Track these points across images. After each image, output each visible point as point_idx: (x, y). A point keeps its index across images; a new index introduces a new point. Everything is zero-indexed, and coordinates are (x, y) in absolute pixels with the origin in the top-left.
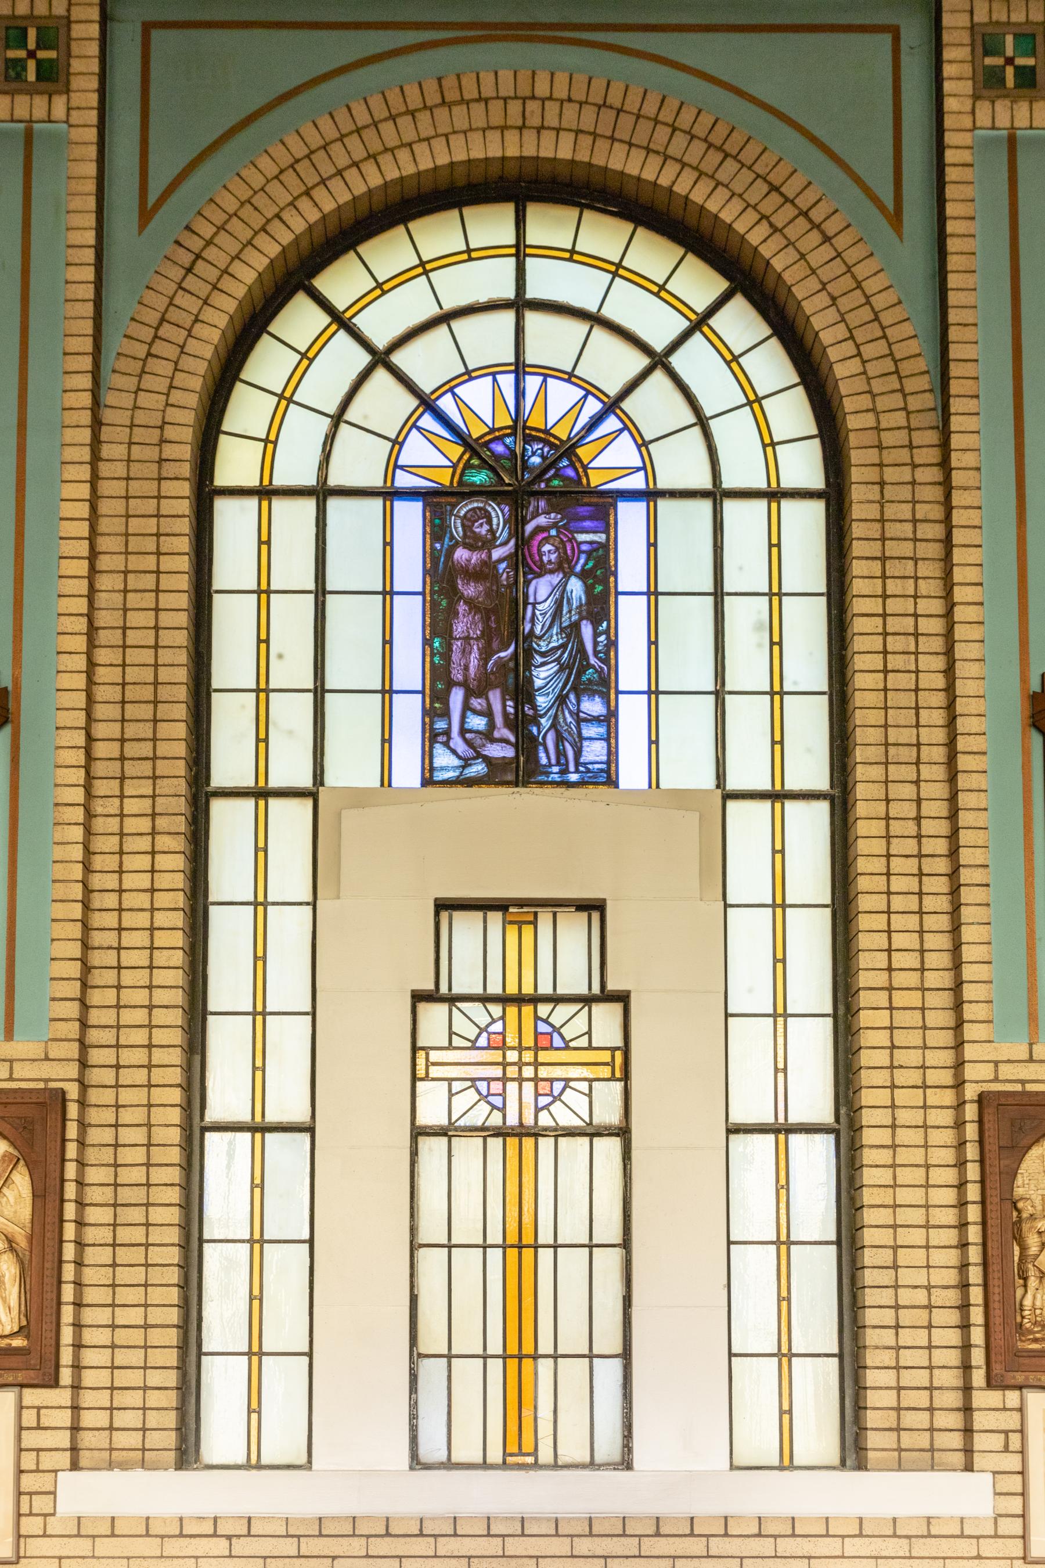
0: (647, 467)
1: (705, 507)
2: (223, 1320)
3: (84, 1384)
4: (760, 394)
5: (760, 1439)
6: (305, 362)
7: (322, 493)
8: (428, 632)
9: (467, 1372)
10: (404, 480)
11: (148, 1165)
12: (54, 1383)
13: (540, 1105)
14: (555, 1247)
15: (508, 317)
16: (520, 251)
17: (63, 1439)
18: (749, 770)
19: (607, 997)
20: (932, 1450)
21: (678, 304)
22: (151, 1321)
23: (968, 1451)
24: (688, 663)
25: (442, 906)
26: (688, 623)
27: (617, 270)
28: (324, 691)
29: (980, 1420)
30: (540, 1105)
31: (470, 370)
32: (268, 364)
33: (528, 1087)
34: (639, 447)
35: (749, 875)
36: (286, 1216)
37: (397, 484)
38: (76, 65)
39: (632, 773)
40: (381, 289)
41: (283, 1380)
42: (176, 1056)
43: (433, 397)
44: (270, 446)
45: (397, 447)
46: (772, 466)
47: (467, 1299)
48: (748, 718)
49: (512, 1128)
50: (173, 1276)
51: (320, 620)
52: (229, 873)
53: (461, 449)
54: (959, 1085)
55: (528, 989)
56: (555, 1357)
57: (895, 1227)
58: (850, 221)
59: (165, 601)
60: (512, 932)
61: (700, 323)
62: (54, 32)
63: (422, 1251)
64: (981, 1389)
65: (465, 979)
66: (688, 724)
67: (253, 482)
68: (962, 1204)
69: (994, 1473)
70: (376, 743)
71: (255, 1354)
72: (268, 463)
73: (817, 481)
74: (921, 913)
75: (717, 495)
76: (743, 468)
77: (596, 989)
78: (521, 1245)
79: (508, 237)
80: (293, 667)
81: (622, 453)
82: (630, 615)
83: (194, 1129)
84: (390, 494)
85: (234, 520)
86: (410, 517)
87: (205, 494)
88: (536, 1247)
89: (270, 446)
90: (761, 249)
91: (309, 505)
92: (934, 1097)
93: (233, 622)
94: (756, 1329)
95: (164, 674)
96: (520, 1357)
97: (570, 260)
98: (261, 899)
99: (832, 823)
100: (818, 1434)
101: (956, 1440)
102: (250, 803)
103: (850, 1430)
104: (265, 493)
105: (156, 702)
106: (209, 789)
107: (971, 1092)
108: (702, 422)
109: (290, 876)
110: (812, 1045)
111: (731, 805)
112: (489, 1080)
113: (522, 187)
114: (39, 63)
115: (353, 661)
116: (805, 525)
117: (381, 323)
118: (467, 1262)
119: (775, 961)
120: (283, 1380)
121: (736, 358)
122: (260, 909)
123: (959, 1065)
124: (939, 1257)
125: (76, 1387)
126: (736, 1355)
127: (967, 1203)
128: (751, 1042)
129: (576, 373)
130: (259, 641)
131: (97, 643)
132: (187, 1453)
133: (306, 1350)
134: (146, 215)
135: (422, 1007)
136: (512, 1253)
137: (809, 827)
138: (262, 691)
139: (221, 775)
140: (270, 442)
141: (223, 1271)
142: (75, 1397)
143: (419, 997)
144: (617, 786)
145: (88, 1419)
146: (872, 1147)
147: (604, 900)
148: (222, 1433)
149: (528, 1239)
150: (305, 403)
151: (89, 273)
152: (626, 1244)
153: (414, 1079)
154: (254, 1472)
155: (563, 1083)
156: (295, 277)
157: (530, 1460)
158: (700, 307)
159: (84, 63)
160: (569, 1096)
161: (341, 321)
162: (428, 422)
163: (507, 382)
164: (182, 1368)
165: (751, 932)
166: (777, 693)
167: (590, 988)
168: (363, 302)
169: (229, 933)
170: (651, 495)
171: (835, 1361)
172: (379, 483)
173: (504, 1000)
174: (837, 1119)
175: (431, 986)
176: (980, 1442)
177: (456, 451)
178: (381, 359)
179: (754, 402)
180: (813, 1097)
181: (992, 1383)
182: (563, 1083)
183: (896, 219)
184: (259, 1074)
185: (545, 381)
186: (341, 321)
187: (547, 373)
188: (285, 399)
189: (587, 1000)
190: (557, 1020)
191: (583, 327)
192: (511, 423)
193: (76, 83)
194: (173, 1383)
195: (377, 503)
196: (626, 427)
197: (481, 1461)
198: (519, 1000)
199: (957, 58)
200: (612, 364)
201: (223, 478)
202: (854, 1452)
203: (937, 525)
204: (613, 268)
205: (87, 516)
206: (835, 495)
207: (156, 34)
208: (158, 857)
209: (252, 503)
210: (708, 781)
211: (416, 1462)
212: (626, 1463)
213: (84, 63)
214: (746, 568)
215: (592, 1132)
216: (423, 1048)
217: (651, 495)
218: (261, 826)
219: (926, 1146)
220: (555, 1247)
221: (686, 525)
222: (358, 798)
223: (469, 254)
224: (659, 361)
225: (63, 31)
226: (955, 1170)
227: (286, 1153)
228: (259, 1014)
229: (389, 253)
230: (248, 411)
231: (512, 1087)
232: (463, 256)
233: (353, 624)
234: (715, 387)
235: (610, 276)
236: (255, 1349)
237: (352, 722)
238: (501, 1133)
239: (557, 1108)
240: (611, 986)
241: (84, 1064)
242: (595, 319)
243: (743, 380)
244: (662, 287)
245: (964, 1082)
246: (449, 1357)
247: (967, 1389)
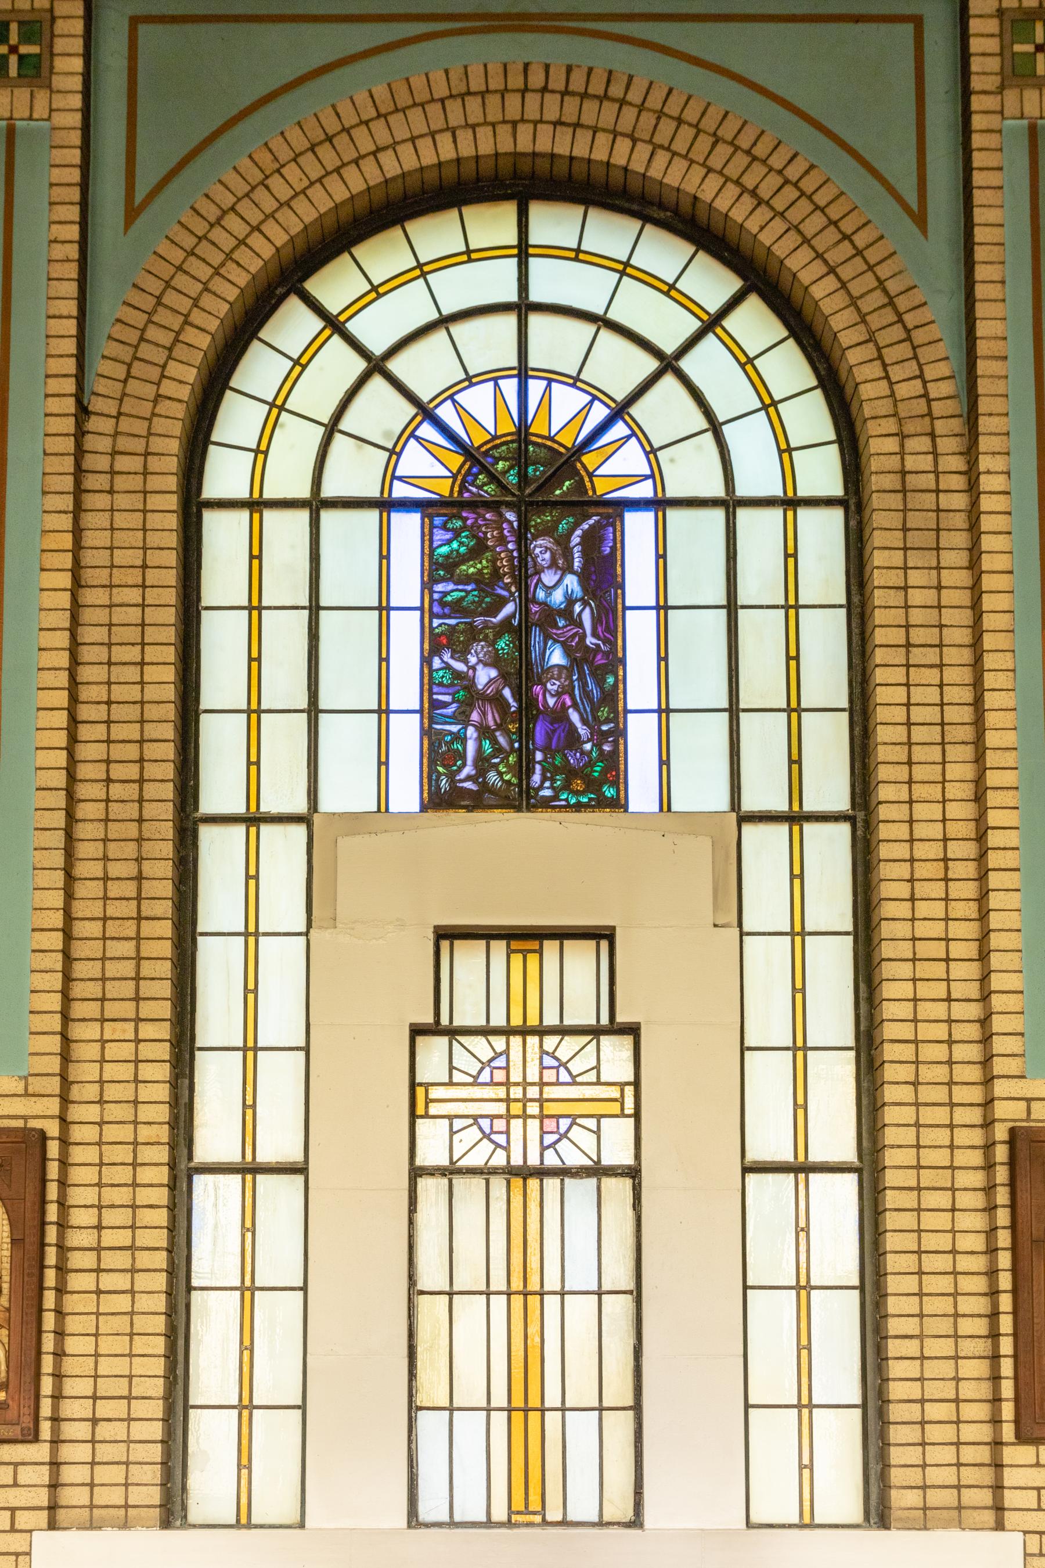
0: (655, 475)
1: (718, 515)
2: (212, 1373)
3: (66, 1393)
4: (776, 398)
5: (776, 1501)
6: (298, 369)
7: (316, 504)
8: (426, 646)
9: (470, 1426)
10: (401, 491)
11: (136, 1102)
12: (36, 1439)
13: (546, 1144)
14: (562, 1294)
15: (510, 321)
16: (523, 251)
17: (42, 1497)
18: (764, 792)
19: (616, 1029)
20: (960, 1508)
21: (687, 304)
22: (139, 1265)
23: (999, 1508)
24: (700, 680)
25: (446, 935)
26: (700, 637)
27: (624, 269)
28: (319, 608)
29: (1010, 1477)
30: (546, 1144)
31: (471, 380)
32: (260, 371)
33: (534, 1125)
34: (647, 454)
35: (766, 901)
36: (278, 1261)
37: (395, 495)
38: (60, 64)
39: (641, 791)
40: (377, 292)
41: (275, 1434)
42: (164, 1072)
43: (432, 405)
44: (261, 457)
45: (394, 457)
46: (788, 473)
47: (470, 1345)
48: (765, 737)
49: (519, 1167)
50: (159, 1323)
51: (321, 652)
52: (219, 903)
53: (461, 459)
54: (988, 1124)
55: (533, 1021)
56: (563, 1409)
57: (924, 1487)
58: (870, 217)
59: (153, 558)
60: (517, 960)
61: (712, 324)
62: (38, 27)
63: (421, 1414)
64: (1013, 1444)
65: (468, 1012)
66: (701, 742)
67: (244, 494)
68: (992, 1250)
69: (1025, 1532)
70: (372, 762)
71: (246, 1407)
72: (258, 475)
73: (837, 490)
74: (946, 880)
75: (730, 504)
76: (758, 474)
77: (605, 1020)
78: (526, 1294)
79: (511, 237)
80: (284, 684)
81: (630, 460)
82: (639, 633)
83: (182, 1172)
84: (386, 505)
85: (224, 536)
86: (407, 527)
87: (192, 508)
88: (543, 1410)
89: (261, 457)
90: (774, 248)
91: (303, 516)
92: (959, 1010)
93: (222, 639)
94: (774, 1377)
95: (147, 969)
96: (526, 1410)
97: (576, 259)
98: (255, 603)
99: (853, 786)
100: (841, 1491)
101: (985, 1497)
102: (245, 514)
103: (875, 1468)
104: (256, 505)
105: (140, 820)
106: (198, 815)
107: (1001, 1133)
108: (715, 427)
109: (283, 903)
110: (835, 1080)
111: (747, 829)
112: (492, 1117)
113: (522, 183)
114: (22, 58)
115: (347, 679)
116: (823, 534)
117: (376, 328)
118: (470, 1427)
119: (788, 658)
120: (275, 1434)
121: (751, 361)
122: (255, 613)
123: (988, 1103)
124: (963, 1137)
125: (56, 1442)
126: (750, 1049)
127: (997, 1249)
128: (768, 1076)
129: (582, 377)
130: (250, 660)
131: (85, 448)
132: (172, 1511)
133: (303, 1044)
134: (132, 213)
135: (420, 1040)
136: (517, 1301)
137: (830, 849)
138: (255, 608)
139: (205, 1151)
140: (261, 452)
141: (213, 1322)
142: (54, 1452)
143: (417, 1031)
144: (626, 811)
145: (69, 1474)
146: (897, 1337)
147: (614, 928)
148: (210, 1486)
149: (534, 1285)
150: (296, 412)
151: (70, 327)
152: (637, 1408)
153: (413, 1116)
154: (244, 1531)
155: (568, 1121)
156: (289, 277)
157: (538, 1519)
158: (713, 307)
159: (69, 66)
160: (576, 1133)
161: (335, 325)
162: (427, 431)
163: (510, 387)
164: (168, 1419)
165: (769, 960)
166: (792, 607)
167: (598, 1020)
168: (358, 305)
169: (218, 965)
170: (659, 504)
171: (856, 1293)
172: (376, 494)
173: (507, 1032)
174: (860, 1156)
175: (429, 1019)
176: (1011, 1498)
177: (456, 461)
178: (377, 366)
179: (770, 405)
180: (835, 1136)
181: (1022, 1438)
182: (568, 1121)
183: (920, 219)
184: (251, 986)
185: (549, 385)
186: (335, 325)
187: (551, 377)
188: (277, 407)
189: (595, 1032)
190: (563, 1054)
191: (590, 329)
192: (514, 430)
193: (58, 82)
194: (158, 1436)
195: (372, 516)
196: (634, 434)
197: (484, 1519)
198: (524, 1032)
199: (984, 41)
200: (619, 367)
201: (211, 490)
202: (878, 1513)
203: (986, 1469)
204: (621, 267)
205: (64, 745)
206: (853, 501)
207: (143, 29)
208: (149, 572)
209: (240, 830)
210: (722, 803)
211: (413, 1518)
212: (636, 1522)
213: (69, 66)
214: (761, 578)
215: (597, 1171)
216: (420, 1084)
217: (659, 504)
218: (253, 787)
219: (946, 899)
220: (562, 1294)
221: (697, 535)
222: (353, 822)
223: (469, 255)
224: (669, 364)
225: (46, 26)
226: (980, 1046)
227: (279, 1195)
228: (250, 1049)
229: (384, 256)
230: (238, 420)
231: (516, 1125)
232: (461, 258)
233: (347, 640)
234: (729, 391)
235: (618, 275)
236: (254, 716)
237: (347, 742)
238: (510, 1172)
239: (564, 1146)
240: (621, 1018)
241: (65, 1100)
242: (602, 322)
243: (759, 384)
244: (672, 287)
245: (994, 1121)
246: (451, 1294)
247: (997, 1444)
